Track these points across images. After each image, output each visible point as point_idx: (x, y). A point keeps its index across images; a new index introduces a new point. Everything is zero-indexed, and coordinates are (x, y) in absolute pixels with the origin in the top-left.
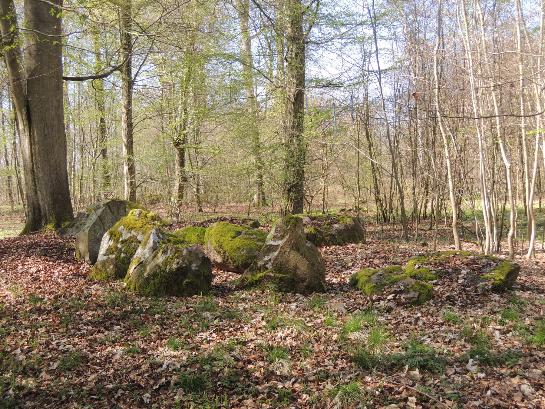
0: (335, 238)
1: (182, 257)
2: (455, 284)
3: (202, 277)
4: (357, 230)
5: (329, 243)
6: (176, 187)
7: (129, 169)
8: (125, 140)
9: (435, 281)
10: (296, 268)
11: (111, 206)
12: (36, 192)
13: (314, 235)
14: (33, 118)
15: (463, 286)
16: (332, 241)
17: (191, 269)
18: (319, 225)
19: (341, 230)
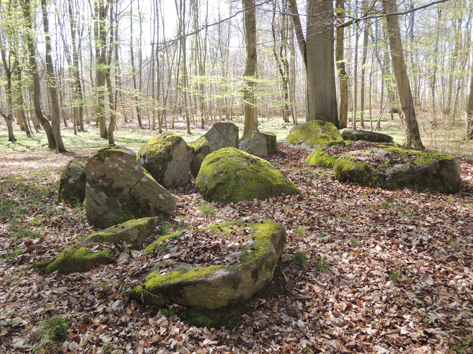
14: (307, 59)
16: (380, 183)
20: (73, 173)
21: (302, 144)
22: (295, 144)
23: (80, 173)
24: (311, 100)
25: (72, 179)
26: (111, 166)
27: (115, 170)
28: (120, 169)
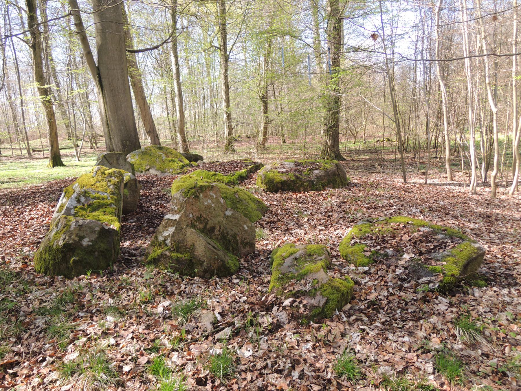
0: (313, 184)
1: (68, 232)
2: (390, 276)
3: (96, 253)
4: (339, 175)
5: (307, 188)
6: (262, 128)
7: (227, 116)
8: (224, 97)
9: (366, 268)
10: (193, 247)
11: (108, 158)
12: (111, 140)
13: (293, 181)
14: (104, 83)
15: (400, 279)
16: (310, 187)
17: (82, 245)
18: (300, 171)
19: (320, 176)
20: (86, 231)
21: (151, 170)
22: (142, 172)
23: (97, 229)
24: (113, 126)
25: (87, 239)
26: (206, 204)
27: (209, 207)
28: (213, 205)
